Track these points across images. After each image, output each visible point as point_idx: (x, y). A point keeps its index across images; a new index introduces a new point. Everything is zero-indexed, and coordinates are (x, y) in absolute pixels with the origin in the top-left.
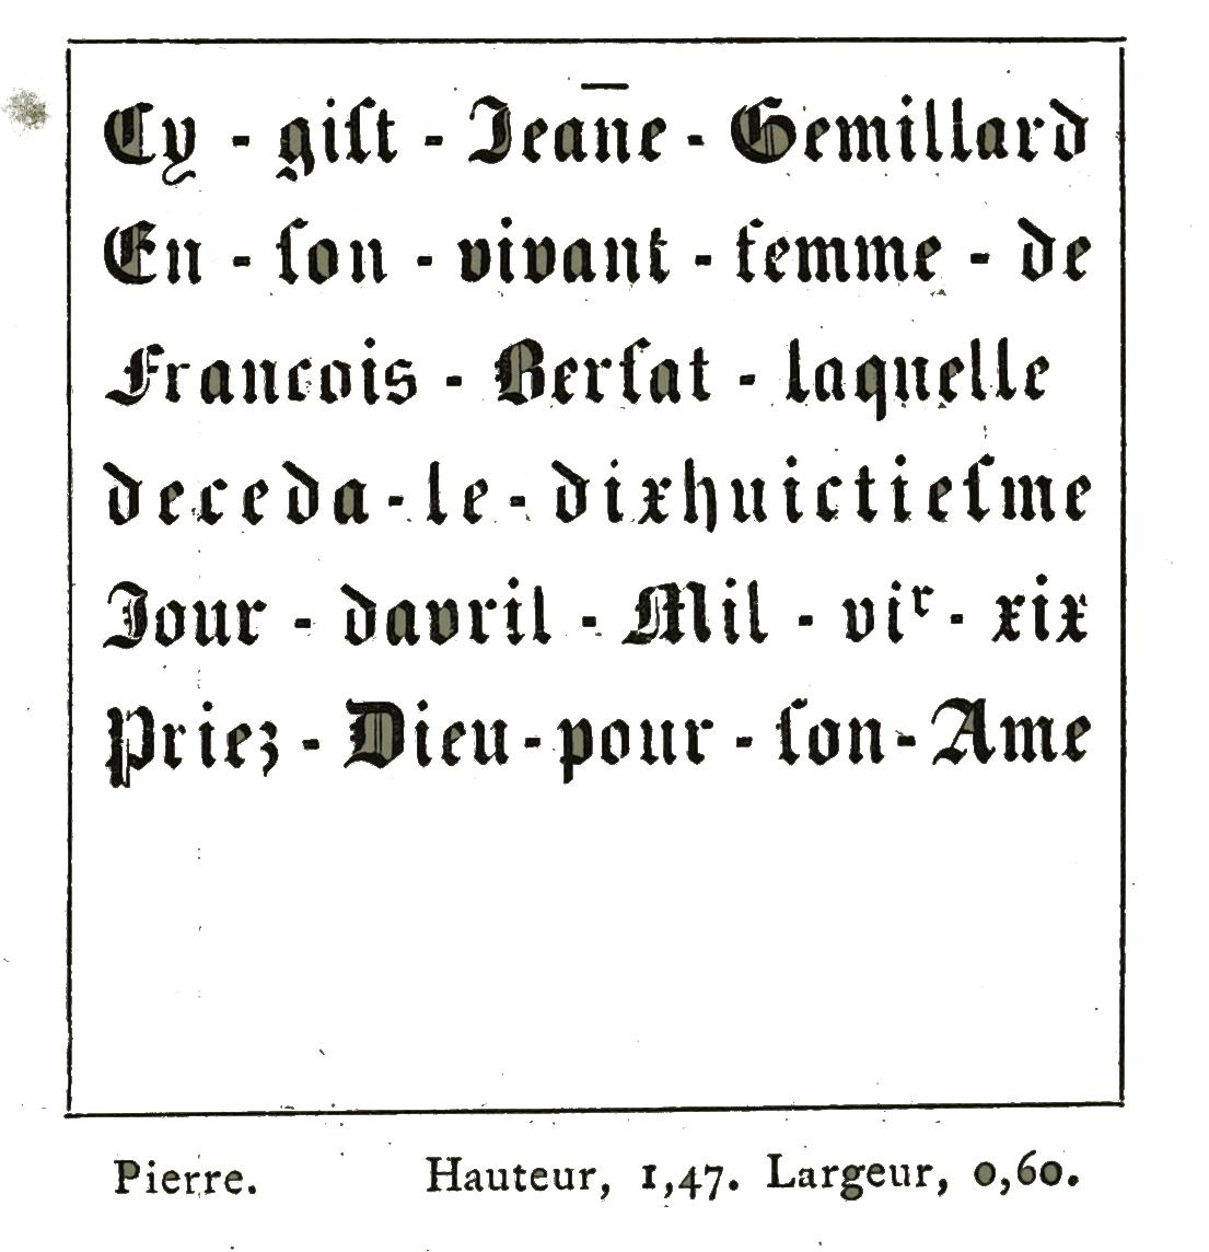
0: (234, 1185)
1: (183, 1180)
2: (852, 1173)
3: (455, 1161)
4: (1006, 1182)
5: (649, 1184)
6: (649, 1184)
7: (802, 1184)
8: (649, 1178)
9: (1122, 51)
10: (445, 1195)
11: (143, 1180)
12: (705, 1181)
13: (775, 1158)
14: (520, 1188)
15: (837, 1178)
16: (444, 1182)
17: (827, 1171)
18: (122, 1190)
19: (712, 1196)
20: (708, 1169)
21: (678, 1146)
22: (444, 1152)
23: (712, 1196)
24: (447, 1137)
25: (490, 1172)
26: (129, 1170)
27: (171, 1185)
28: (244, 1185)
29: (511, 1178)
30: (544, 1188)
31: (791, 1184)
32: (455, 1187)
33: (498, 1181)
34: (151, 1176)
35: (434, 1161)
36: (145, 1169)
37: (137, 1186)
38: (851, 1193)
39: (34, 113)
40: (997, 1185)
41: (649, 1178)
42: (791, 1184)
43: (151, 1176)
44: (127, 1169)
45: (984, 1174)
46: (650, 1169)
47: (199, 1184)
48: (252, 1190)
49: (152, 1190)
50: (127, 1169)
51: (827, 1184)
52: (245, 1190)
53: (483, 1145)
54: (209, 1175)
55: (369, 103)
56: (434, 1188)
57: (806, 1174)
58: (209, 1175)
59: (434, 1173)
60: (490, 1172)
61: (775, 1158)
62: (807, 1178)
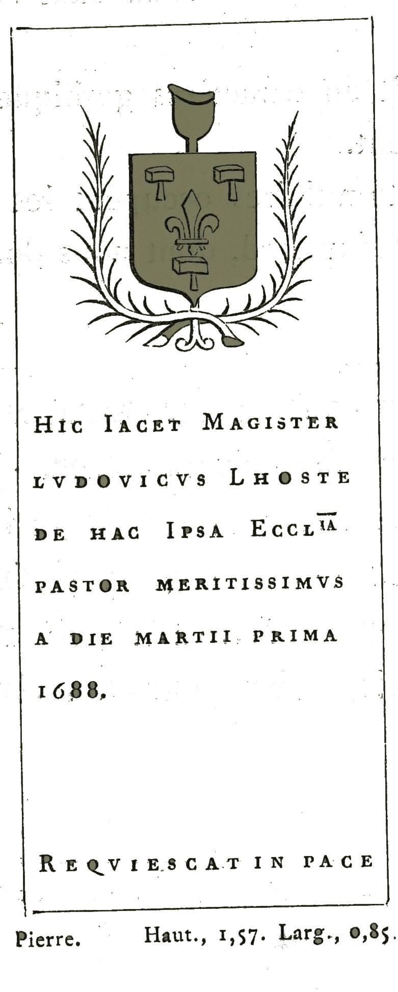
0: (69, 942)
1: (46, 940)
2: (319, 932)
3: (157, 928)
4: (365, 937)
5: (223, 939)
6: (223, 939)
7: (295, 938)
8: (223, 935)
9: (18, 29)
10: (153, 944)
11: (28, 941)
12: (249, 937)
13: (282, 926)
14: (189, 940)
15: (311, 935)
16: (153, 938)
17: (307, 931)
18: (19, 945)
19: (252, 943)
20: (250, 931)
21: (233, 922)
22: (43, 414)
23: (252, 943)
24: (152, 920)
25: (175, 933)
26: (22, 936)
27: (41, 943)
28: (74, 942)
29: (184, 936)
30: (71, 945)
31: (290, 938)
32: (157, 940)
33: (178, 937)
34: (31, 939)
35: (147, 928)
36: (29, 936)
37: (25, 943)
38: (318, 941)
39: (43, 425)
40: (361, 938)
41: (223, 935)
42: (290, 938)
43: (31, 939)
44: (21, 936)
45: (355, 933)
46: (223, 932)
47: (53, 942)
48: (78, 944)
49: (31, 946)
50: (21, 936)
51: (307, 938)
52: (75, 945)
53: (168, 923)
54: (58, 938)
55: (257, 419)
56: (148, 941)
57: (297, 933)
58: (58, 938)
59: (148, 934)
60: (175, 933)
61: (282, 926)
62: (297, 935)
